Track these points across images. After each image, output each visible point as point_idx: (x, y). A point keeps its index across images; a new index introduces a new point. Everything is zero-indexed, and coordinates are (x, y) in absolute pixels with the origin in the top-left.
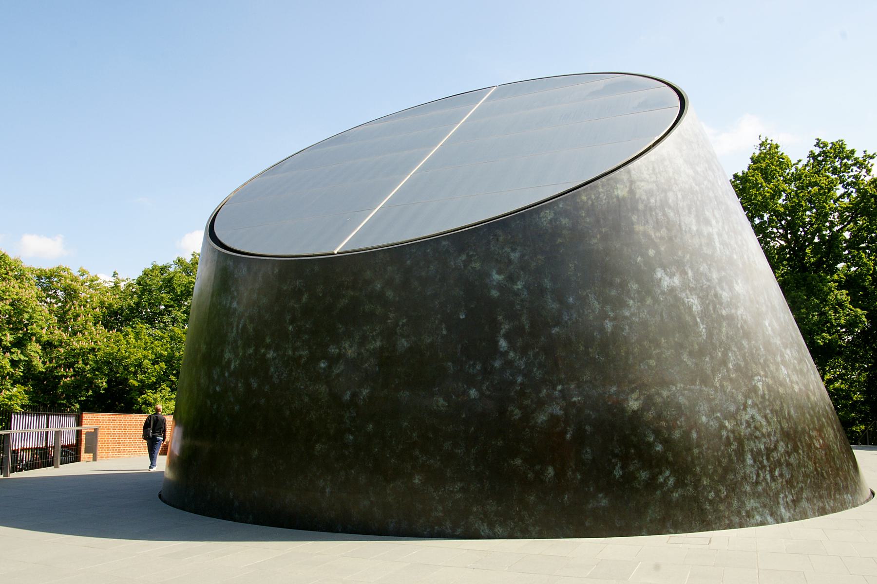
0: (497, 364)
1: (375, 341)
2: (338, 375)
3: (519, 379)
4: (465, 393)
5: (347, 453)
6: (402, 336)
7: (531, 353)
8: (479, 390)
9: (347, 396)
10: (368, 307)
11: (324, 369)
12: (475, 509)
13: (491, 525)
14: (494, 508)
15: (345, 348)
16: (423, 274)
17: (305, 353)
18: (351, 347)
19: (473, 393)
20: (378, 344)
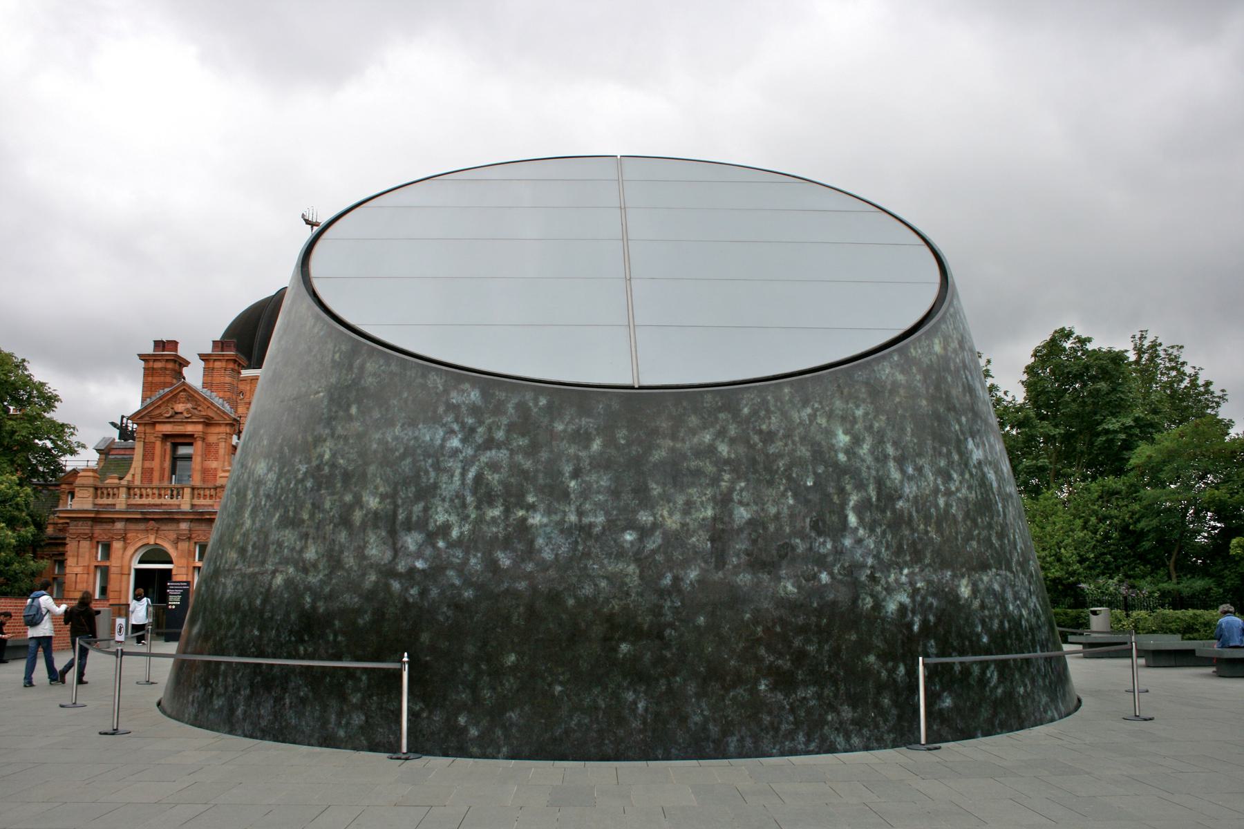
0: (848, 542)
1: (706, 509)
2: (654, 552)
3: (870, 561)
4: (815, 577)
5: (669, 655)
6: (741, 503)
7: (879, 530)
8: (831, 574)
9: (667, 581)
10: (693, 464)
11: (631, 542)
12: (830, 718)
13: (848, 738)
14: (850, 715)
15: (662, 516)
16: (764, 427)
17: (600, 519)
18: (671, 514)
19: (824, 577)
20: (709, 513)
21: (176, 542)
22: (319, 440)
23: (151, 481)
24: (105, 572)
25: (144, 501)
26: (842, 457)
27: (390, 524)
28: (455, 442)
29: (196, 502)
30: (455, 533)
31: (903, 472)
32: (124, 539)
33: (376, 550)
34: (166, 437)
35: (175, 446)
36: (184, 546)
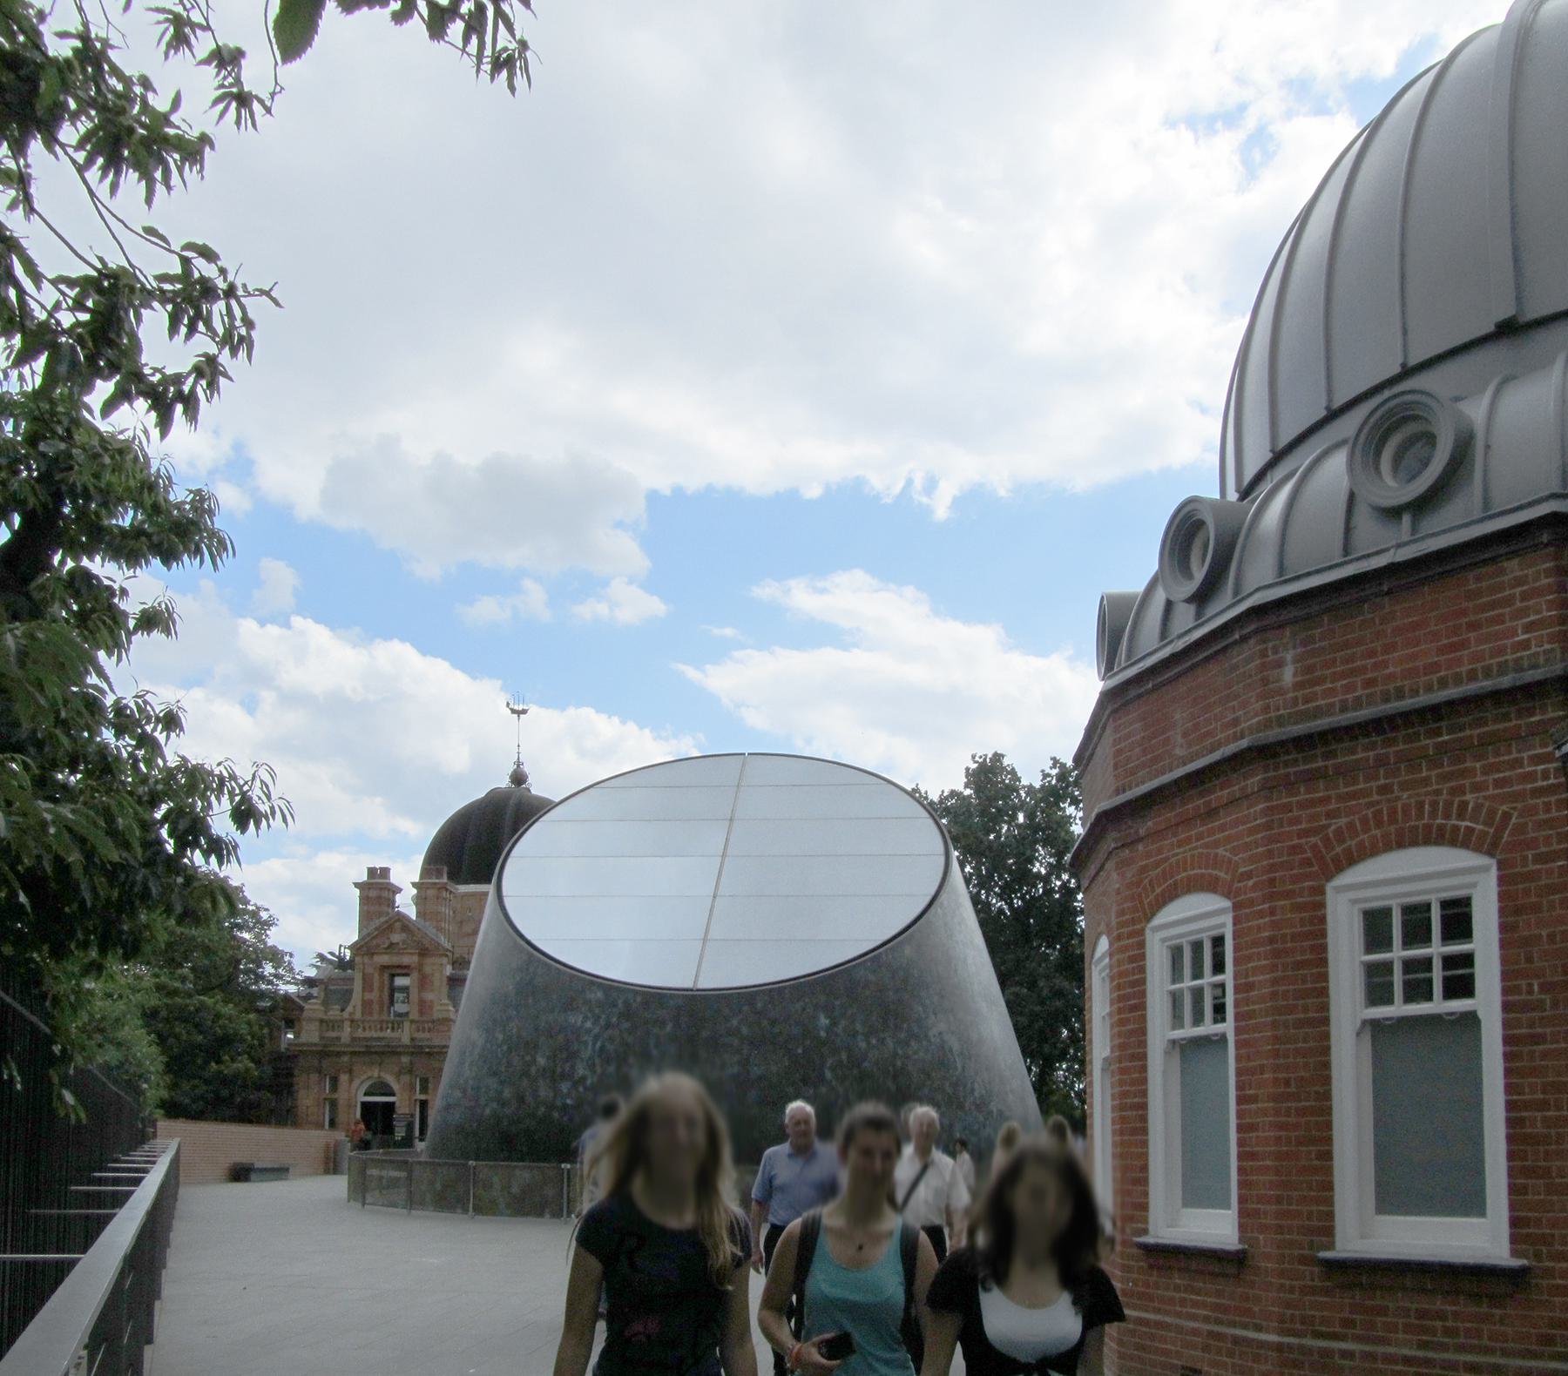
21: (398, 1075)
22: (509, 1018)
23: (371, 1014)
24: (334, 1104)
25: (368, 1034)
26: (823, 1034)
27: (553, 1077)
28: (588, 1024)
29: (416, 1035)
30: (589, 1082)
31: (869, 1043)
32: (350, 1071)
33: (544, 1092)
34: (384, 968)
35: (393, 976)
36: (406, 1078)
